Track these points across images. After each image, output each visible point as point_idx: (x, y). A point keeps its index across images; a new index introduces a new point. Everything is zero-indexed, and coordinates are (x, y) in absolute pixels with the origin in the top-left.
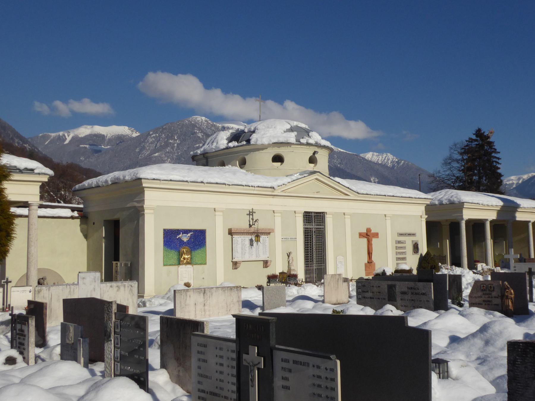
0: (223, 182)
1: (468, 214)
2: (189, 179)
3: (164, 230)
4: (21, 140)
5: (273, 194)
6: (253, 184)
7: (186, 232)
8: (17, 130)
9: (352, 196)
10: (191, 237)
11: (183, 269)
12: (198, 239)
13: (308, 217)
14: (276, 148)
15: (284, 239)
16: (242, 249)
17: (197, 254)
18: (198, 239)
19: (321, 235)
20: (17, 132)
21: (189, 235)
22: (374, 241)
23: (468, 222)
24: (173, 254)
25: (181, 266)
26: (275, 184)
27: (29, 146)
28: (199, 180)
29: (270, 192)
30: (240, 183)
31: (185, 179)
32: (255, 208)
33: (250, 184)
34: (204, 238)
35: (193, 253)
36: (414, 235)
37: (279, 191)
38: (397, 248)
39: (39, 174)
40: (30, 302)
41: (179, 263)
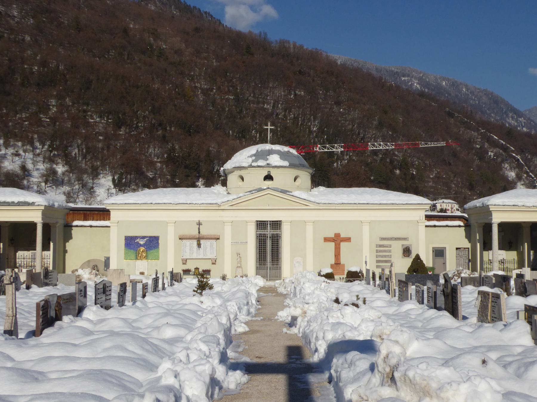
0: (169, 202)
1: (497, 218)
2: (140, 202)
3: (126, 237)
4: (515, 114)
5: (220, 208)
6: (197, 202)
7: (143, 237)
8: (510, 102)
9: (312, 206)
10: (146, 242)
11: (139, 262)
12: (153, 243)
13: (261, 225)
14: (239, 171)
15: (234, 243)
16: (190, 250)
17: (152, 252)
18: (153, 243)
19: (276, 240)
20: (511, 105)
21: (145, 240)
22: (344, 246)
23: (502, 226)
24: (132, 253)
25: (138, 261)
26: (219, 201)
27: (524, 119)
28: (149, 202)
29: (217, 207)
30: (185, 202)
31: (137, 202)
32: (201, 220)
33: (194, 202)
34: (158, 243)
35: (148, 252)
36: (405, 239)
37: (226, 206)
38: (377, 251)
39: (38, 205)
40: (526, 305)
41: (137, 259)
